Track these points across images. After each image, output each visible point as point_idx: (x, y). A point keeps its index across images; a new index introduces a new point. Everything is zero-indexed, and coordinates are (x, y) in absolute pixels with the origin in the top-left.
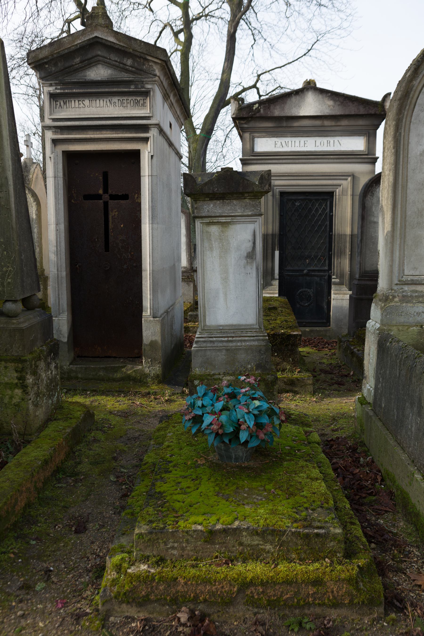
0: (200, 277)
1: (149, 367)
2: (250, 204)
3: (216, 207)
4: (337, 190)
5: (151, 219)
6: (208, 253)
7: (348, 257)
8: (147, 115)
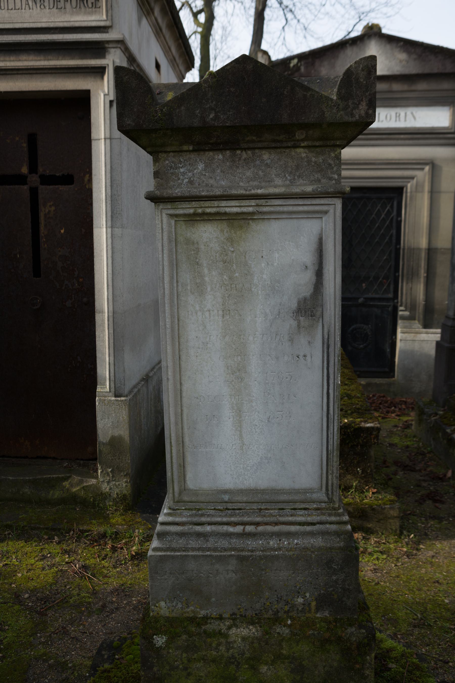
0: (170, 364)
1: (110, 482)
2: (309, 162)
3: (214, 171)
4: (409, 185)
5: (109, 218)
6: (191, 299)
7: (422, 280)
8: (102, 24)
